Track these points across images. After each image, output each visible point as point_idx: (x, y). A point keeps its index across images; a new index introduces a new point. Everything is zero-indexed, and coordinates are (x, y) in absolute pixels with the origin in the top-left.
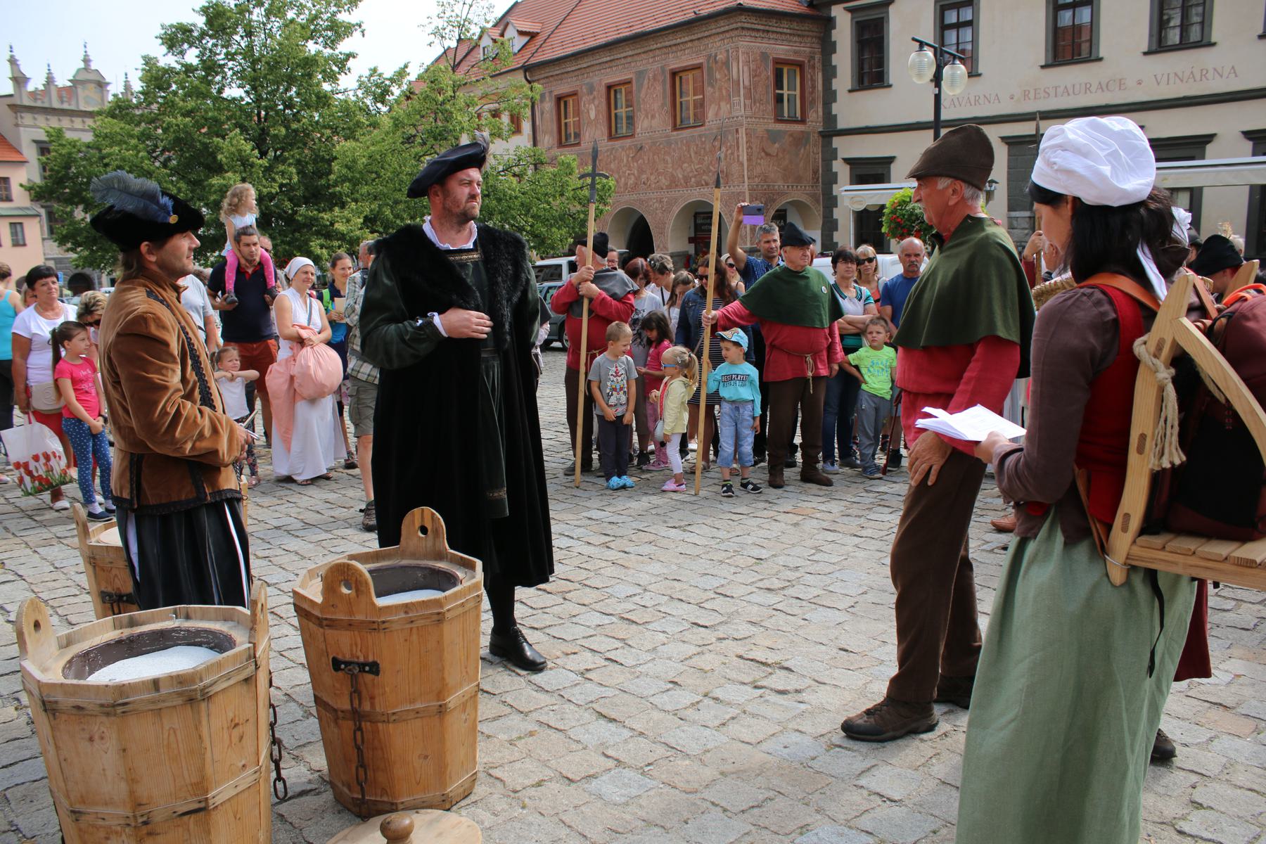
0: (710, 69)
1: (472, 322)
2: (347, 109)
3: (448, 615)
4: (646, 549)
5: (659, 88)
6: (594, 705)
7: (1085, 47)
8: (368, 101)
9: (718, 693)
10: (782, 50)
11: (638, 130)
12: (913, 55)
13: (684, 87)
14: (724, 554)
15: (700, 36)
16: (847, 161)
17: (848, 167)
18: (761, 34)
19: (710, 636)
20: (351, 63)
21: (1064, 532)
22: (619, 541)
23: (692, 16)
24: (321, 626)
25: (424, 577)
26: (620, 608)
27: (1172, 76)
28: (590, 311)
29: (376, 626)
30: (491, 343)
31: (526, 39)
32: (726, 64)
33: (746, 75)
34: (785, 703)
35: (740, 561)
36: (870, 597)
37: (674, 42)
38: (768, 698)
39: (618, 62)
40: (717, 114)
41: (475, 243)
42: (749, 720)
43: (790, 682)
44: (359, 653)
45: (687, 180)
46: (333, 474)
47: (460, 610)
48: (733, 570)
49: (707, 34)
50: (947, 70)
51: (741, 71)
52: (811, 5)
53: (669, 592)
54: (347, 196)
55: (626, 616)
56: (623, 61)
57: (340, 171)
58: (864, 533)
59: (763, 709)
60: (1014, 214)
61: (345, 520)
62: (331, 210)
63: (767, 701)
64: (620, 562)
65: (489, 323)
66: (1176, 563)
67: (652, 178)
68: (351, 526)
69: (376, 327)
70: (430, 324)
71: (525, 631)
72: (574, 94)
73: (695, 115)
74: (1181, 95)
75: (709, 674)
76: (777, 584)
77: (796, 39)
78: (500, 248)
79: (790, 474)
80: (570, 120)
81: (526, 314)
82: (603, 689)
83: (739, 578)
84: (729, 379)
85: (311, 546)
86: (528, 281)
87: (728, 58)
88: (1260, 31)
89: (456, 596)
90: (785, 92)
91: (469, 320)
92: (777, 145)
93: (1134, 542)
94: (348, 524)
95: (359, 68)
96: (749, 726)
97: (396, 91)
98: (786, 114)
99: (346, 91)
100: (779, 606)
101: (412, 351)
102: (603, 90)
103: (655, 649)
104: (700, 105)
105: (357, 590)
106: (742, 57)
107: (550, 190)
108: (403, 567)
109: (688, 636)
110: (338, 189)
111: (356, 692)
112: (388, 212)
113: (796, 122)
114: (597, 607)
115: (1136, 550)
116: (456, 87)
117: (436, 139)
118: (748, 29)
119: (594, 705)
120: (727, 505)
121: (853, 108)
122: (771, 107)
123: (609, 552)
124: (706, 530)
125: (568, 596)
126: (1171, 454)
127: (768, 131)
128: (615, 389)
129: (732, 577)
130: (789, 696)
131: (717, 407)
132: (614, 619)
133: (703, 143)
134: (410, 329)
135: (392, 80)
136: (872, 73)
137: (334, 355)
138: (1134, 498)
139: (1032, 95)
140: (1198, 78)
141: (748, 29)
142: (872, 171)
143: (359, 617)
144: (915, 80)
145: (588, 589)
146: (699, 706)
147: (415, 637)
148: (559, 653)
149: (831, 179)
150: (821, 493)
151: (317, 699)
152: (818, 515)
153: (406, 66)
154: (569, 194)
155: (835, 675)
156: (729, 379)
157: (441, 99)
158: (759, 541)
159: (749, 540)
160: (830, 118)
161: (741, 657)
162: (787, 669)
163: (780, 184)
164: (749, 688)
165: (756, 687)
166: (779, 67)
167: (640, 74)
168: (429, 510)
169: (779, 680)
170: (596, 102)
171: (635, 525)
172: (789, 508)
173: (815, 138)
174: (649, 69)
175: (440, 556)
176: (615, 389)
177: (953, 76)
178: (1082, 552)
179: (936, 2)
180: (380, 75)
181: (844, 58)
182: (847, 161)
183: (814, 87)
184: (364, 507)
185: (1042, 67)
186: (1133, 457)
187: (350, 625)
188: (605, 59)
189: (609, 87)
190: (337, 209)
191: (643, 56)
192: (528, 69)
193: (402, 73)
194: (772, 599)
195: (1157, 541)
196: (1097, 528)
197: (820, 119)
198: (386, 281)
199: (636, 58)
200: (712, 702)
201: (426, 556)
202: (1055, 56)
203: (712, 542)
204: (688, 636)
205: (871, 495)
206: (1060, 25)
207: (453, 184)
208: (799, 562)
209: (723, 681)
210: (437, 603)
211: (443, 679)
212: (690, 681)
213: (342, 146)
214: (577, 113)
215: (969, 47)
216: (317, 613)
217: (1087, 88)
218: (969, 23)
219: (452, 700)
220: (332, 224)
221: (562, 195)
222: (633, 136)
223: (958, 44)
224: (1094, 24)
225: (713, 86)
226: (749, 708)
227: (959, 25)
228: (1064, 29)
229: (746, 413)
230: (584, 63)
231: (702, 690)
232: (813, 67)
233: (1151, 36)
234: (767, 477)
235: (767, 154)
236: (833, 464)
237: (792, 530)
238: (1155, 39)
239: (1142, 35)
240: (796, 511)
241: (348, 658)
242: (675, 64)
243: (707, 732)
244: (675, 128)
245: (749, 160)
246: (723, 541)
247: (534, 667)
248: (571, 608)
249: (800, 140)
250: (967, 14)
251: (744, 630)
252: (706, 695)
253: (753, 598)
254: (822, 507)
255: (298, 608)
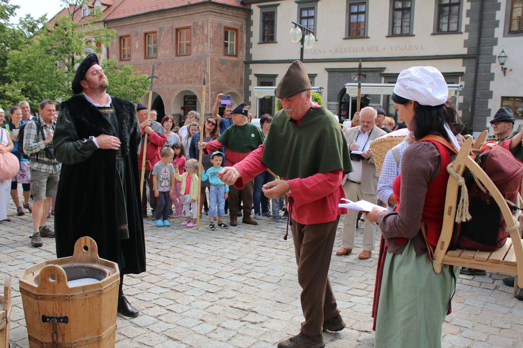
0: (194, 29)
1: (109, 141)
2: (15, 35)
3: (105, 291)
4: (178, 256)
5: (170, 36)
6: (165, 333)
7: (362, 32)
8: (25, 31)
9: (224, 324)
10: (228, 22)
11: (159, 55)
12: (292, 29)
13: (182, 36)
14: (216, 257)
15: (190, 13)
16: (256, 75)
17: (256, 78)
18: (219, 14)
19: (215, 297)
20: (16, 11)
21: (416, 250)
22: (164, 252)
23: (187, 3)
24: (37, 299)
25: (86, 272)
26: (170, 284)
27: (397, 47)
28: (148, 141)
29: (68, 297)
30: (120, 152)
31: (105, 7)
32: (202, 27)
33: (211, 33)
34: (257, 328)
35: (224, 261)
36: (287, 277)
37: (178, 15)
38: (248, 326)
39: (150, 22)
40: (197, 50)
41: (111, 104)
42: (241, 337)
43: (258, 319)
44: (57, 312)
45: (181, 80)
46: (11, 218)
47: (110, 289)
48: (221, 265)
49: (193, 12)
50: (306, 37)
51: (209, 31)
52: (242, 3)
53: (192, 276)
54: (13, 78)
55: (173, 288)
56: (153, 22)
57: (11, 65)
58: (279, 247)
59: (246, 332)
60: (330, 103)
61: (22, 242)
62: (4, 84)
63: (248, 327)
64: (166, 262)
65: (120, 142)
66: (464, 263)
67: (165, 78)
68: (25, 245)
69: (62, 143)
70: (91, 141)
71: (127, 297)
72: (129, 36)
73: (186, 49)
74: (401, 55)
75: (218, 316)
76: (243, 272)
77: (235, 18)
78: (124, 108)
79: (240, 219)
80: (126, 48)
81: (135, 139)
82: (169, 325)
83: (225, 269)
84: (213, 174)
85: (4, 256)
86: (136, 123)
87: (203, 24)
88: (432, 32)
89: (108, 281)
90: (229, 42)
91: (110, 140)
92: (224, 66)
93: (446, 254)
94: (23, 244)
95: (21, 14)
96: (242, 340)
97: (40, 26)
98: (229, 52)
99: (13, 24)
100: (245, 282)
101: (81, 155)
102: (143, 35)
103: (190, 304)
104: (188, 45)
105: (58, 280)
106: (210, 24)
107: (119, 81)
108: (75, 267)
109: (205, 297)
110: (8, 74)
111: (55, 332)
112: (37, 87)
113: (233, 56)
114: (159, 284)
115: (447, 258)
116: (74, 27)
117: (62, 53)
118: (213, 12)
119: (165, 333)
120: (213, 234)
121: (260, 51)
122: (222, 48)
123: (160, 257)
124: (205, 246)
125: (143, 279)
126: (466, 215)
127: (220, 59)
128: (164, 179)
129: (221, 269)
130: (258, 325)
131: (207, 188)
132: (168, 290)
133: (190, 63)
134: (80, 144)
135: (38, 21)
136: (269, 36)
137: (15, 158)
138: (446, 234)
139: (339, 51)
140: (408, 48)
141: (213, 12)
142: (266, 80)
143: (59, 294)
144: (293, 41)
145: (153, 276)
146: (216, 331)
147: (87, 303)
148: (144, 308)
149: (248, 83)
150: (256, 229)
151: (30, 337)
152: (256, 239)
153: (46, 15)
154: (129, 84)
155: (277, 314)
156: (213, 174)
157: (66, 33)
158: (231, 251)
159: (226, 251)
160: (249, 55)
161: (232, 307)
162: (254, 312)
163: (225, 84)
164: (238, 322)
165: (241, 321)
166: (226, 31)
167: (161, 29)
168: (89, 238)
169: (251, 317)
170: (139, 41)
171: (170, 244)
172: (242, 236)
173: (242, 64)
174: (165, 27)
175: (94, 261)
176: (164, 179)
177: (309, 40)
178: (423, 258)
179: (347, 2)
180: (32, 18)
181: (256, 28)
182: (256, 75)
183: (242, 40)
184: (32, 235)
185: (387, 37)
186: (446, 217)
187: (53, 298)
188: (144, 21)
189: (146, 34)
190: (7, 84)
191: (163, 20)
192: (106, 22)
193: (43, 18)
194: (242, 279)
195: (457, 252)
196: (430, 248)
197: (245, 55)
198: (67, 121)
199: (159, 21)
200: (222, 329)
201: (87, 262)
202: (349, 34)
203: (209, 252)
204: (205, 297)
205: (278, 229)
206: (352, 21)
207: (89, 75)
208: (251, 261)
209: (225, 319)
210: (100, 285)
211: (101, 323)
212: (210, 319)
213: (13, 53)
214: (130, 45)
215: (312, 27)
216: (35, 292)
217: (363, 50)
218: (313, 17)
219: (104, 334)
220: (4, 92)
221: (125, 84)
222: (156, 58)
223: (307, 26)
224: (365, 23)
225: (195, 37)
226: (240, 331)
227: (308, 18)
228: (353, 23)
229: (222, 191)
230: (134, 21)
231: (217, 323)
232: (242, 32)
233: (389, 29)
234: (229, 221)
235: (220, 70)
236: (259, 215)
237: (245, 246)
238: (391, 31)
239: (385, 29)
240: (246, 237)
241: (51, 315)
242: (178, 26)
243: (222, 344)
244: (177, 55)
245: (211, 72)
246: (214, 251)
247: (133, 315)
248: (146, 285)
249: (235, 65)
250: (362, 8)
251: (231, 294)
252: (218, 326)
253: (233, 278)
254: (258, 235)
255: (22, 290)
